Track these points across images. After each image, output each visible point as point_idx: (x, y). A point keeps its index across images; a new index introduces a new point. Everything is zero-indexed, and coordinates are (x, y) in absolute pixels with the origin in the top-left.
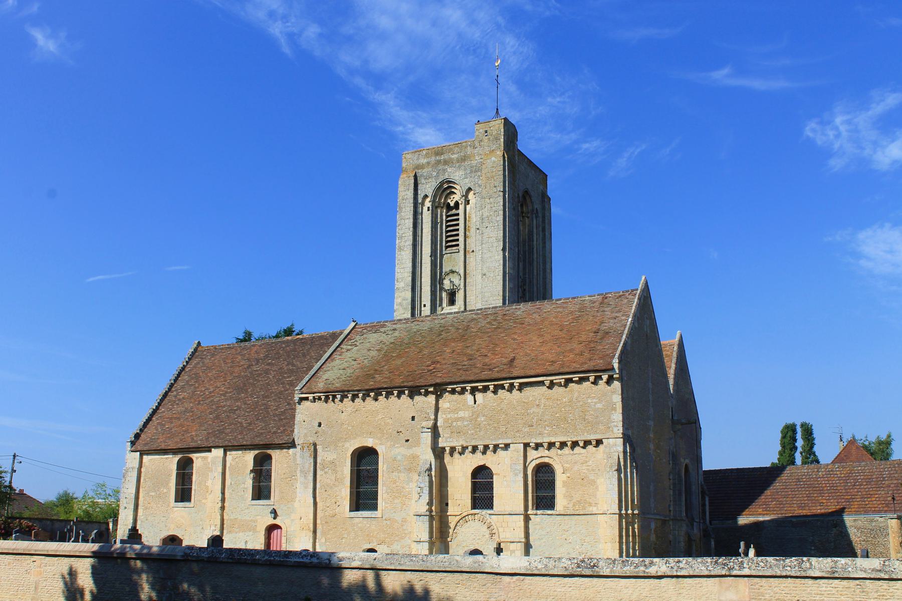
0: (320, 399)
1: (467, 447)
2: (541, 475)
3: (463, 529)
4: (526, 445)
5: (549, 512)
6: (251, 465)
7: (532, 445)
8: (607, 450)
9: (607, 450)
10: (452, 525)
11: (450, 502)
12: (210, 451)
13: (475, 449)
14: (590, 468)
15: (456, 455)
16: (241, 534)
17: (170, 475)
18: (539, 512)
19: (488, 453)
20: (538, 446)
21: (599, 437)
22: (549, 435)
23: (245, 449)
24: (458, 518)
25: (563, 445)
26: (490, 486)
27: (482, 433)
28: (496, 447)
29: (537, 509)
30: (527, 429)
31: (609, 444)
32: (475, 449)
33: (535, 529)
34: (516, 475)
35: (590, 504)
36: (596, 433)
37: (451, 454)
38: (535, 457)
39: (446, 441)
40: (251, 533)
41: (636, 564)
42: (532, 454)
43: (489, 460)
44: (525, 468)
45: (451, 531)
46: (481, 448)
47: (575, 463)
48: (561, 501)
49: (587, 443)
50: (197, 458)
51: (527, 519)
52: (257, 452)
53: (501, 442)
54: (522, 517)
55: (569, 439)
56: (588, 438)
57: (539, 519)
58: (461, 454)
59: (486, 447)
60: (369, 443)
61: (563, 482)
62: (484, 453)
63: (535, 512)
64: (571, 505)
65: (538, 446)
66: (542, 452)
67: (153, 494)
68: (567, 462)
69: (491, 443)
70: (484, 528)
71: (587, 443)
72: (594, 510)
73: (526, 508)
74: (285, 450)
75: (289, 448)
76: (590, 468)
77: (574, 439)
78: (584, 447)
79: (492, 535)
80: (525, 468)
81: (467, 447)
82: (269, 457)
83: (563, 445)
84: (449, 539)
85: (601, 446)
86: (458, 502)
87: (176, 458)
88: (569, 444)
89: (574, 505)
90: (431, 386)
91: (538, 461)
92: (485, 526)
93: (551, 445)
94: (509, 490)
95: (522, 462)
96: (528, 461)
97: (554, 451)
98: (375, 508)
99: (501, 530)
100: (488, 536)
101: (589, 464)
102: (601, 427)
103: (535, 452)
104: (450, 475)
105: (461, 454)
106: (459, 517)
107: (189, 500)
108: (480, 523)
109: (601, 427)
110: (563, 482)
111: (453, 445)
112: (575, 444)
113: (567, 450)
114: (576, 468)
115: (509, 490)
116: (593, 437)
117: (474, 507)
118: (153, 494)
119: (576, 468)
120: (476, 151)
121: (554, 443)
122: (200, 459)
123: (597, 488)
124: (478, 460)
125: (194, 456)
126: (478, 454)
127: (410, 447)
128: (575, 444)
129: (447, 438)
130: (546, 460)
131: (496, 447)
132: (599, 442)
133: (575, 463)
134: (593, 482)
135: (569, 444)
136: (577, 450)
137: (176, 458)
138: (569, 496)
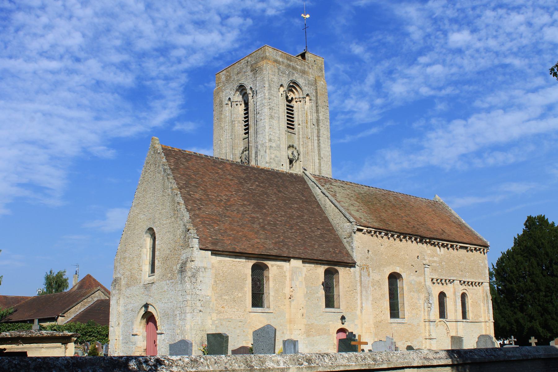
0: (369, 233)
6: (322, 279)
12: (289, 261)
16: (318, 337)
17: (245, 280)
23: (317, 263)
30: (460, 273)
40: (326, 336)
41: (25, 350)
50: (272, 266)
52: (326, 267)
60: (398, 270)
67: (226, 297)
74: (348, 268)
75: (351, 267)
82: (337, 272)
87: (251, 263)
90: (428, 238)
111: (472, 281)
118: (226, 297)
120: (310, 71)
122: (275, 267)
125: (269, 263)
127: (418, 276)
137: (251, 263)
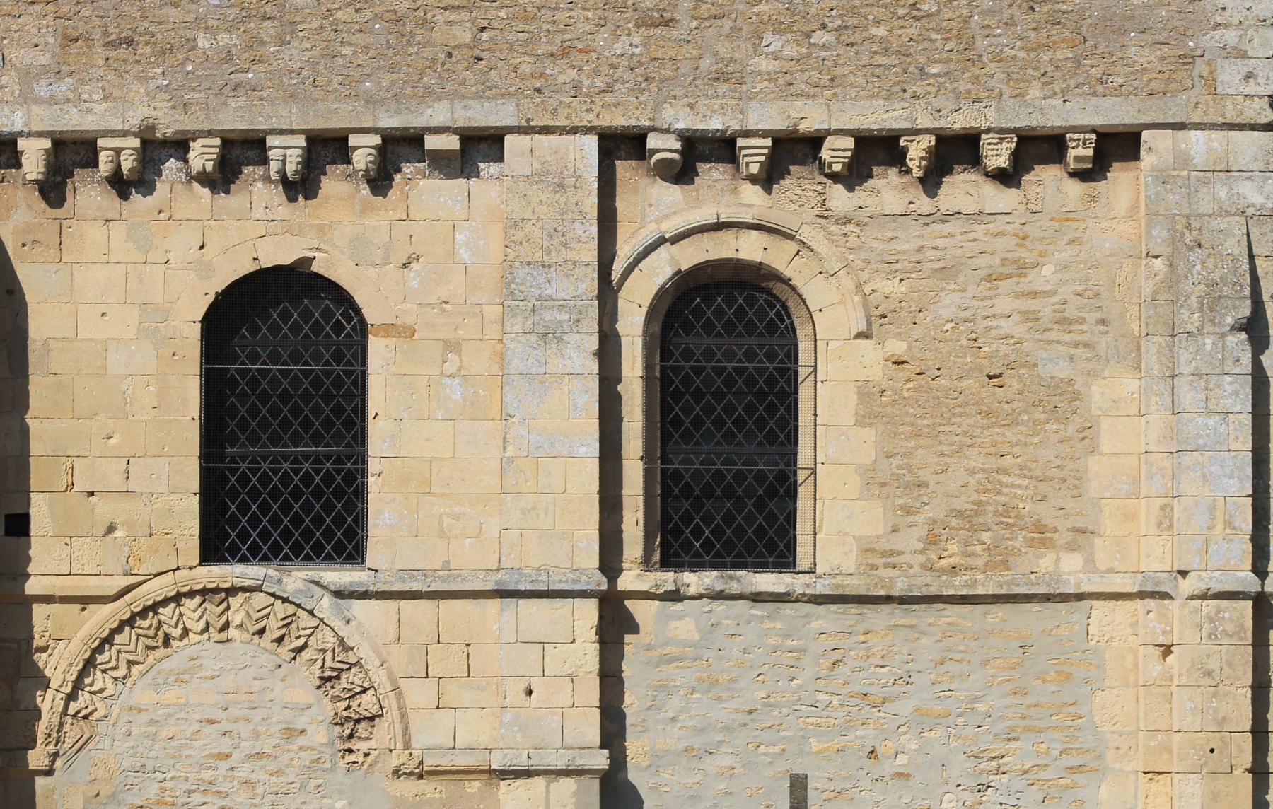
1: (180, 146)
2: (696, 342)
3: (140, 693)
4: (621, 145)
5: (767, 581)
7: (664, 145)
8: (1174, 198)
9: (1174, 198)
10: (58, 664)
11: (40, 510)
13: (240, 154)
14: (1046, 310)
15: (88, 194)
18: (694, 581)
19: (332, 184)
20: (702, 151)
21: (1115, 112)
22: (785, 88)
24: (101, 617)
25: (878, 150)
26: (338, 408)
27: (297, 54)
28: (400, 148)
29: (666, 563)
30: (630, 43)
31: (1183, 160)
32: (240, 154)
33: (663, 688)
34: (549, 336)
35: (1042, 536)
36: (1100, 86)
37: (53, 189)
38: (670, 226)
39: (27, 98)
42: (653, 207)
43: (340, 235)
44: (607, 292)
45: (49, 703)
46: (287, 153)
47: (946, 272)
48: (839, 516)
49: (1037, 148)
51: (615, 623)
53: (442, 116)
54: (588, 612)
55: (919, 117)
56: (1048, 113)
57: (693, 625)
58: (121, 185)
59: (327, 148)
61: (866, 392)
62: (301, 186)
63: (667, 579)
64: (910, 540)
65: (702, 151)
66: (721, 194)
68: (890, 265)
69: (366, 120)
70: (298, 685)
71: (1037, 148)
72: (1070, 570)
73: (610, 561)
76: (1046, 310)
77: (959, 122)
78: (1006, 178)
79: (353, 725)
80: (607, 292)
81: (180, 146)
83: (878, 150)
84: (36, 758)
85: (1119, 174)
86: (104, 509)
88: (917, 151)
89: (932, 541)
91: (690, 255)
92: (305, 674)
93: (793, 151)
94: (494, 430)
95: (589, 253)
96: (625, 250)
97: (799, 188)
98: (779, 552)
99: (418, 694)
100: (320, 735)
101: (1035, 280)
102: (1141, 54)
103: (670, 193)
104: (42, 325)
105: (121, 185)
106: (120, 610)
107: (8, 517)
108: (263, 655)
109: (1141, 54)
110: (866, 392)
111: (74, 121)
112: (956, 150)
113: (888, 191)
114: (948, 304)
115: (494, 430)
116: (1082, 113)
117: (214, 548)
119: (948, 304)
121: (814, 142)
123: (1088, 433)
124: (256, 231)
126: (257, 194)
128: (956, 150)
129: (29, 76)
130: (750, 248)
131: (400, 148)
132: (1118, 146)
133: (946, 272)
134: (1064, 399)
135: (917, 151)
136: (962, 189)
138: (895, 484)
